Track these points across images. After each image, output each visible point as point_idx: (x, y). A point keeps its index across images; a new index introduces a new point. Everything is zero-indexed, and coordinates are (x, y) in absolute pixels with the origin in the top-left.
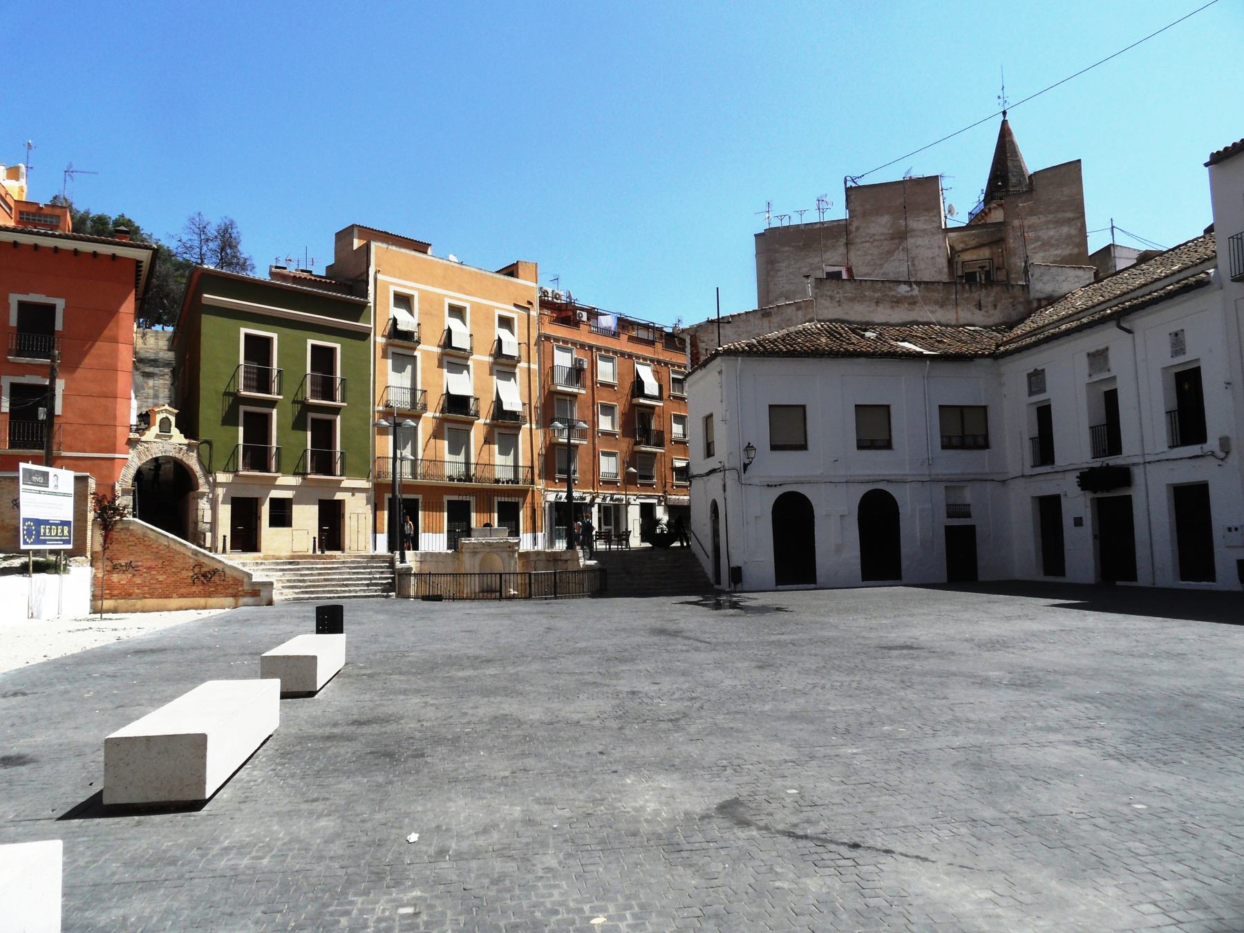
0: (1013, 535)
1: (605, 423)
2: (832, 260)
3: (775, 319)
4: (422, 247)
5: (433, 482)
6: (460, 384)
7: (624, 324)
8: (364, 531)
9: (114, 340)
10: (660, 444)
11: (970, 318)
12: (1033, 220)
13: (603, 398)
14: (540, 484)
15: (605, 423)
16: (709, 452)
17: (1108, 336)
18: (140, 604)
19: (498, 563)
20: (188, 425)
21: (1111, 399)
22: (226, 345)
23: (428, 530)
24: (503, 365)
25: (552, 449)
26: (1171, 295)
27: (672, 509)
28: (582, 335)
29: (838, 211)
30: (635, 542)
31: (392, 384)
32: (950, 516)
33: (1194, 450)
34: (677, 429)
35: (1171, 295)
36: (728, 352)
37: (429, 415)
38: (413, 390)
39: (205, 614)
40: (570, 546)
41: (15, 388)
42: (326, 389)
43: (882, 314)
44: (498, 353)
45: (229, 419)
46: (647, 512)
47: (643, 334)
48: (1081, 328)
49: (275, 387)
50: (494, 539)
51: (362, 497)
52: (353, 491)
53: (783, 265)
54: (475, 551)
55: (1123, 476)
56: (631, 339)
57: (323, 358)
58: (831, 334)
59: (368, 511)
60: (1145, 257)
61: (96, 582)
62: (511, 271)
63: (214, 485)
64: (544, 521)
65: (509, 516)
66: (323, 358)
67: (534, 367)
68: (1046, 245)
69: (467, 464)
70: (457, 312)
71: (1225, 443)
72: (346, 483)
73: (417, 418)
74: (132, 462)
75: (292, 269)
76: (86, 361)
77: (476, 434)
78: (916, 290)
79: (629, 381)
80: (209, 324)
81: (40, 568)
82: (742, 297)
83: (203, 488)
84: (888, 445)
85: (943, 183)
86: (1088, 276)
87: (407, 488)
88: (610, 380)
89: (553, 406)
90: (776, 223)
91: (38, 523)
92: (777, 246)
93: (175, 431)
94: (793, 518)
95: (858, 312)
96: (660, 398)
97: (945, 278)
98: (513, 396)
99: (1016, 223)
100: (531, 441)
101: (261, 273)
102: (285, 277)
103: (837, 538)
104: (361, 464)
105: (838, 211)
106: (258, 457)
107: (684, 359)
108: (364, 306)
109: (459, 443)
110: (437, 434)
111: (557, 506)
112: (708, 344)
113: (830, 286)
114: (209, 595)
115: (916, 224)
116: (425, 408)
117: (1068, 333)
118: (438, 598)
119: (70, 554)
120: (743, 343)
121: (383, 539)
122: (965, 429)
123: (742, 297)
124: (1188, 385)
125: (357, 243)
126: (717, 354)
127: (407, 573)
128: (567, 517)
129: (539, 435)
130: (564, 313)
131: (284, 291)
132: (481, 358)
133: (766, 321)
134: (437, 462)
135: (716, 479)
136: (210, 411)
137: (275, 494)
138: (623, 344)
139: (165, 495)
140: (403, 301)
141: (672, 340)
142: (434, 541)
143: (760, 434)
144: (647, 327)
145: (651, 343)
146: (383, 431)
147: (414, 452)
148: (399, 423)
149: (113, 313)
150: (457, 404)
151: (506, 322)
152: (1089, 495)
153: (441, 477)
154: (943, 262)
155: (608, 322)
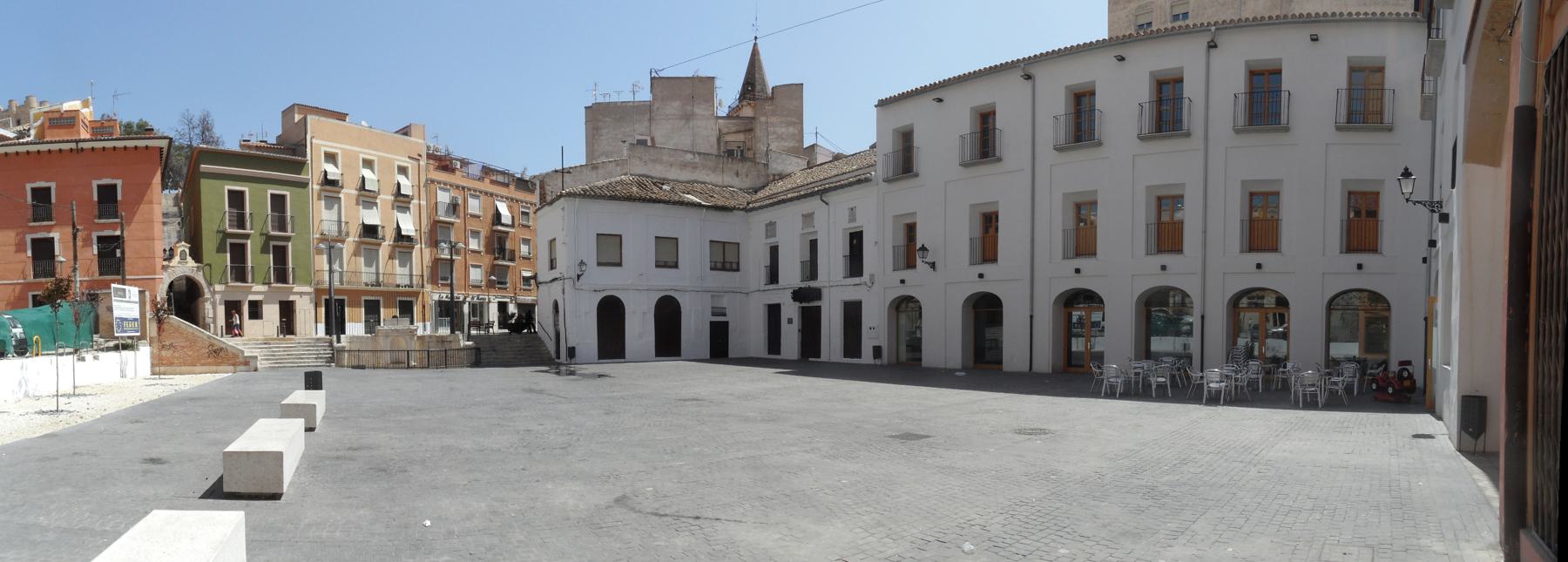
0: (749, 332)
1: (473, 244)
2: (639, 130)
3: (601, 171)
4: (341, 117)
5: (354, 287)
6: (372, 217)
7: (487, 171)
8: (309, 322)
9: (151, 202)
10: (512, 260)
11: (730, 181)
12: (773, 119)
13: (473, 225)
14: (428, 288)
15: (473, 244)
16: (552, 267)
17: (813, 204)
18: (178, 369)
19: (403, 344)
20: (196, 254)
21: (813, 245)
22: (216, 198)
23: (351, 320)
24: (401, 201)
25: (436, 262)
26: (850, 184)
27: (520, 306)
28: (457, 179)
29: (645, 95)
30: (496, 330)
31: (324, 218)
32: (714, 314)
33: (856, 280)
34: (524, 249)
35: (850, 184)
36: (569, 195)
37: (350, 239)
38: (340, 222)
39: (218, 376)
40: (452, 332)
41: (100, 239)
42: (281, 224)
43: (673, 174)
44: (398, 193)
45: (221, 249)
46: (502, 307)
47: (500, 178)
48: (798, 198)
49: (248, 224)
50: (400, 327)
51: (307, 298)
52: (301, 294)
53: (604, 131)
54: (387, 334)
55: (816, 294)
56: (493, 182)
57: (278, 202)
58: (640, 185)
59: (312, 307)
60: (837, 157)
61: (153, 356)
62: (405, 132)
63: (214, 293)
64: (431, 313)
65: (406, 309)
66: (278, 202)
67: (423, 203)
68: (780, 138)
69: (377, 274)
70: (368, 164)
71: (872, 276)
72: (297, 289)
73: (343, 242)
74: (165, 279)
75: (254, 142)
76: (136, 218)
77: (384, 251)
78: (697, 159)
79: (491, 212)
80: (206, 185)
81: (125, 347)
82: (577, 156)
83: (207, 295)
84: (676, 266)
85: (718, 83)
86: (803, 164)
87: (338, 291)
88: (477, 212)
89: (437, 232)
90: (600, 100)
91: (123, 320)
92: (599, 116)
93: (189, 258)
94: (611, 313)
95: (657, 171)
96: (512, 226)
97: (715, 152)
98: (408, 226)
99: (763, 119)
100: (421, 256)
101: (232, 145)
102: (250, 147)
103: (639, 328)
104: (308, 277)
105: (645, 95)
106: (240, 274)
107: (535, 198)
108: (303, 164)
109: (372, 259)
110: (356, 254)
111: (440, 303)
112: (553, 188)
113: (641, 149)
114: (218, 364)
115: (699, 110)
116: (347, 234)
117: (791, 199)
118: (363, 367)
119: (139, 338)
120: (579, 188)
121: (322, 327)
122: (725, 259)
123: (577, 156)
124: (856, 240)
125: (297, 117)
126: (561, 196)
127: (342, 350)
128: (449, 311)
129: (427, 252)
130: (444, 163)
131: (248, 158)
132: (386, 198)
133: (594, 173)
134: (357, 273)
135: (557, 286)
136: (209, 243)
137: (252, 298)
138: (486, 186)
139: (185, 300)
140: (331, 158)
141: (523, 184)
142: (355, 328)
143: (590, 254)
144: (503, 173)
145: (506, 185)
146: (319, 252)
147: (341, 266)
148: (331, 246)
149: (149, 185)
150: (370, 231)
151: (403, 170)
152: (798, 304)
153: (359, 283)
154: (714, 140)
155: (475, 170)
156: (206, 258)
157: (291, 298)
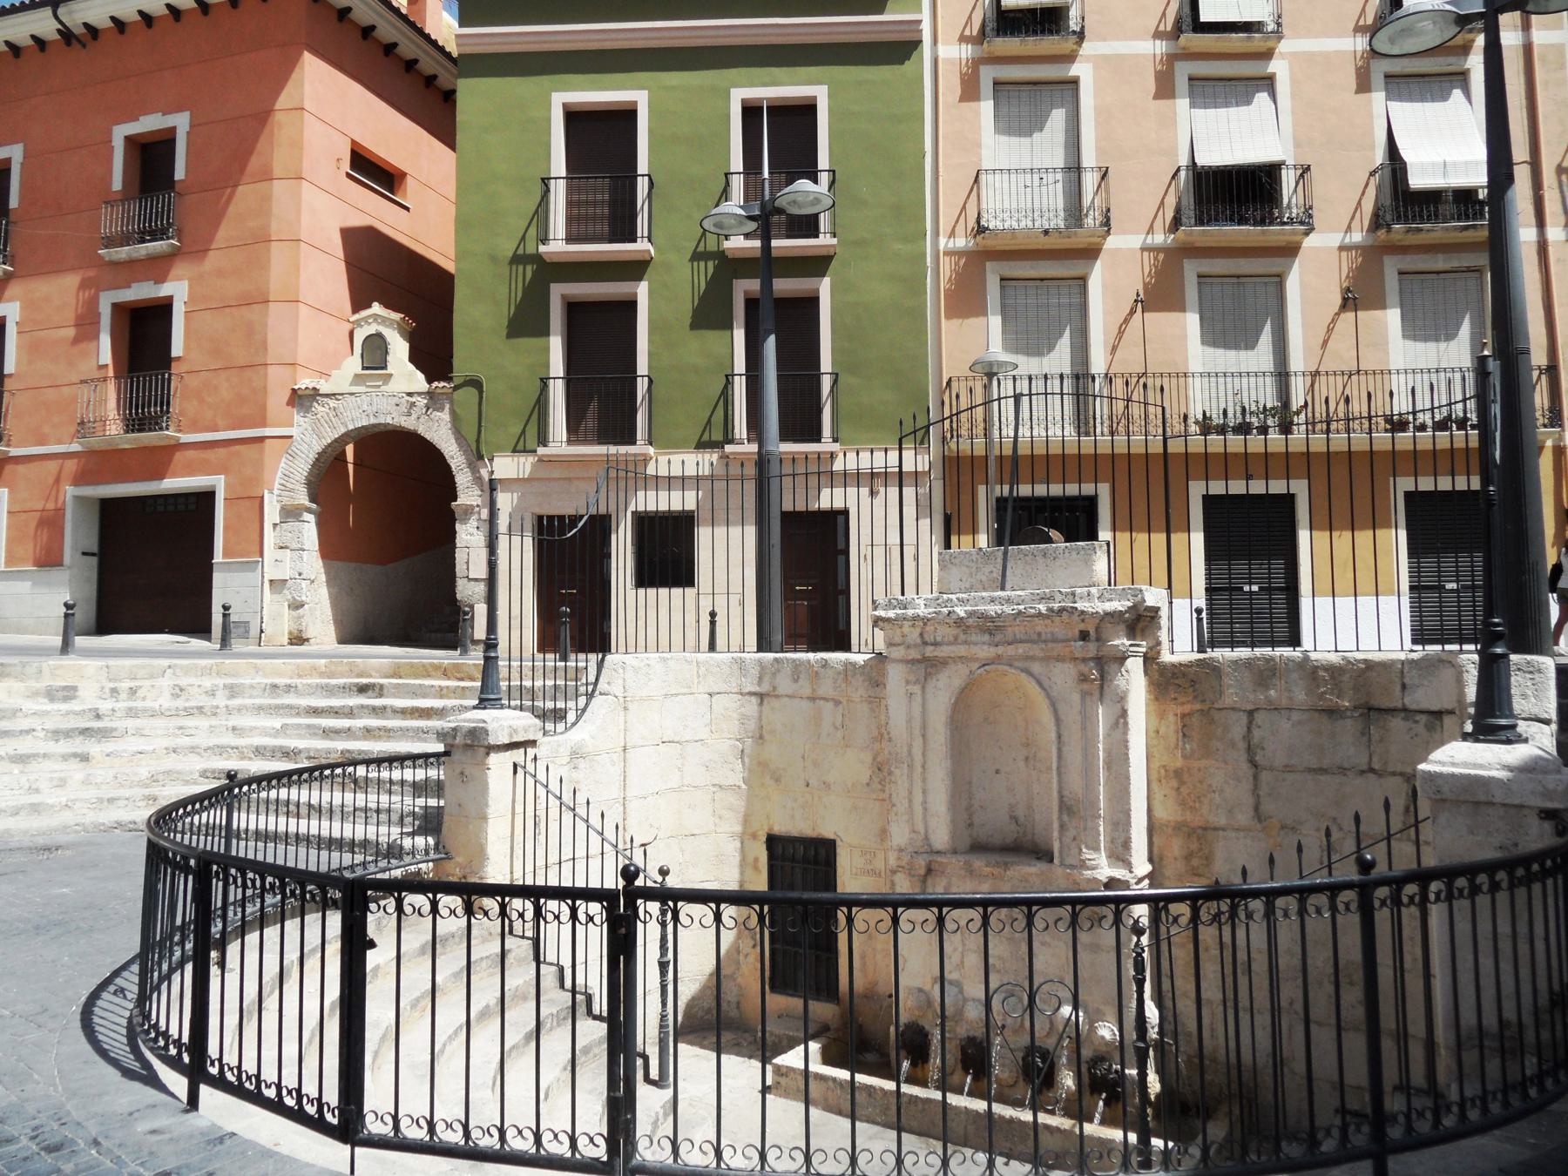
5: (1141, 440)
38: (1074, 169)
52: (872, 479)
66: (786, 135)
76: (223, 234)
77: (1312, 281)
83: (468, 495)
106: (605, 395)
109: (1246, 307)
110: (1160, 294)
148: (1035, 275)
156: (464, 362)
157: (828, 499)
